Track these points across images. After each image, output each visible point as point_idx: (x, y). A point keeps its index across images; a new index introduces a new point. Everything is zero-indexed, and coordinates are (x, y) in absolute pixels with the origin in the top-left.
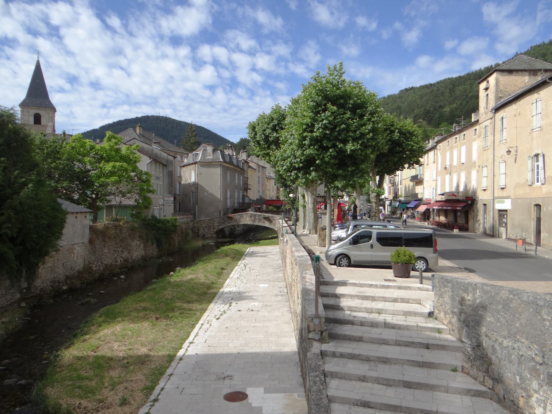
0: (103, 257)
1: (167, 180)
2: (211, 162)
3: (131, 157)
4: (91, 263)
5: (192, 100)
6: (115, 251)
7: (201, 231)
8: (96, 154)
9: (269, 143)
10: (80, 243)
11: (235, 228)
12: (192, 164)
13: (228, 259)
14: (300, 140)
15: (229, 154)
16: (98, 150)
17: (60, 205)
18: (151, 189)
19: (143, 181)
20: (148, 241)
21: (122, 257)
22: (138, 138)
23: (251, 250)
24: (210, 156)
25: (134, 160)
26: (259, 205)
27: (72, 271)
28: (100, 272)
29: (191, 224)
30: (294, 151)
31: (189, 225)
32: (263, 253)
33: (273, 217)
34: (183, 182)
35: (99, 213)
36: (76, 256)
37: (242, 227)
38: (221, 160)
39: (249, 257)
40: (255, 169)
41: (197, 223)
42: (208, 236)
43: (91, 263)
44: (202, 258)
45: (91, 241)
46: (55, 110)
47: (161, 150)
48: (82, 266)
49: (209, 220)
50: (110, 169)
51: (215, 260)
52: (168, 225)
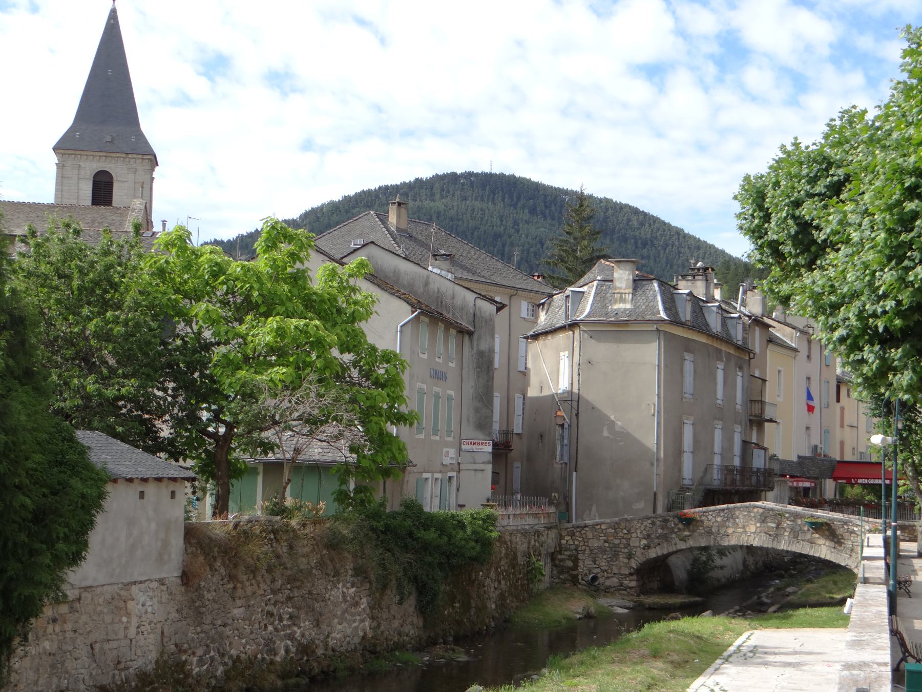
0: (228, 631)
1: (472, 383)
2: (626, 323)
3: (341, 302)
4: (185, 651)
5: (589, 116)
6: (270, 614)
7: (585, 564)
8: (231, 292)
9: (813, 249)
10: (151, 580)
11: (710, 558)
12: (562, 328)
13: (657, 668)
14: (890, 232)
15: (690, 294)
16: (237, 279)
17: (83, 451)
18: (404, 409)
19: (377, 384)
20: (385, 587)
21: (291, 637)
22: (389, 243)
23: (752, 642)
24: (622, 300)
25: (349, 311)
26: (808, 478)
27: (121, 670)
28: (213, 682)
29: (550, 540)
30: (873, 274)
31: (543, 539)
32: (795, 653)
33: (846, 523)
34: (532, 392)
35: (236, 486)
36: (134, 622)
37: (739, 555)
38: (663, 315)
39: (738, 664)
40: (795, 350)
41: (572, 535)
42: (608, 583)
43: (185, 651)
44: (567, 657)
45: (186, 577)
46: (154, 162)
47: (457, 281)
48: (153, 656)
49: (615, 526)
50: (268, 338)
51: (610, 667)
52: (460, 534)
